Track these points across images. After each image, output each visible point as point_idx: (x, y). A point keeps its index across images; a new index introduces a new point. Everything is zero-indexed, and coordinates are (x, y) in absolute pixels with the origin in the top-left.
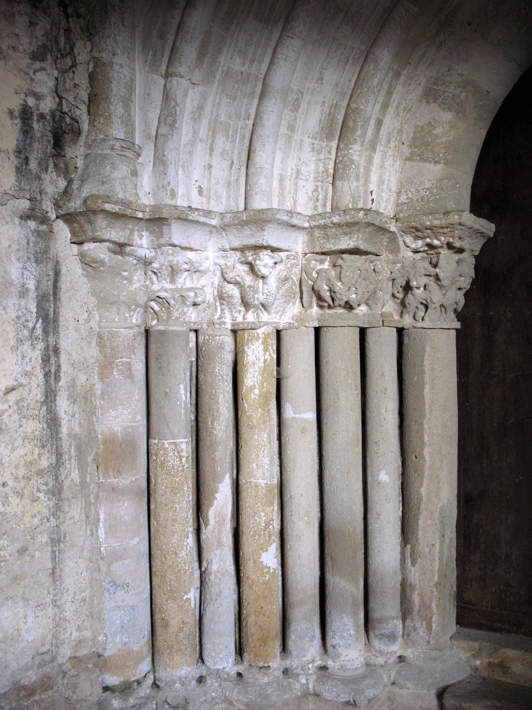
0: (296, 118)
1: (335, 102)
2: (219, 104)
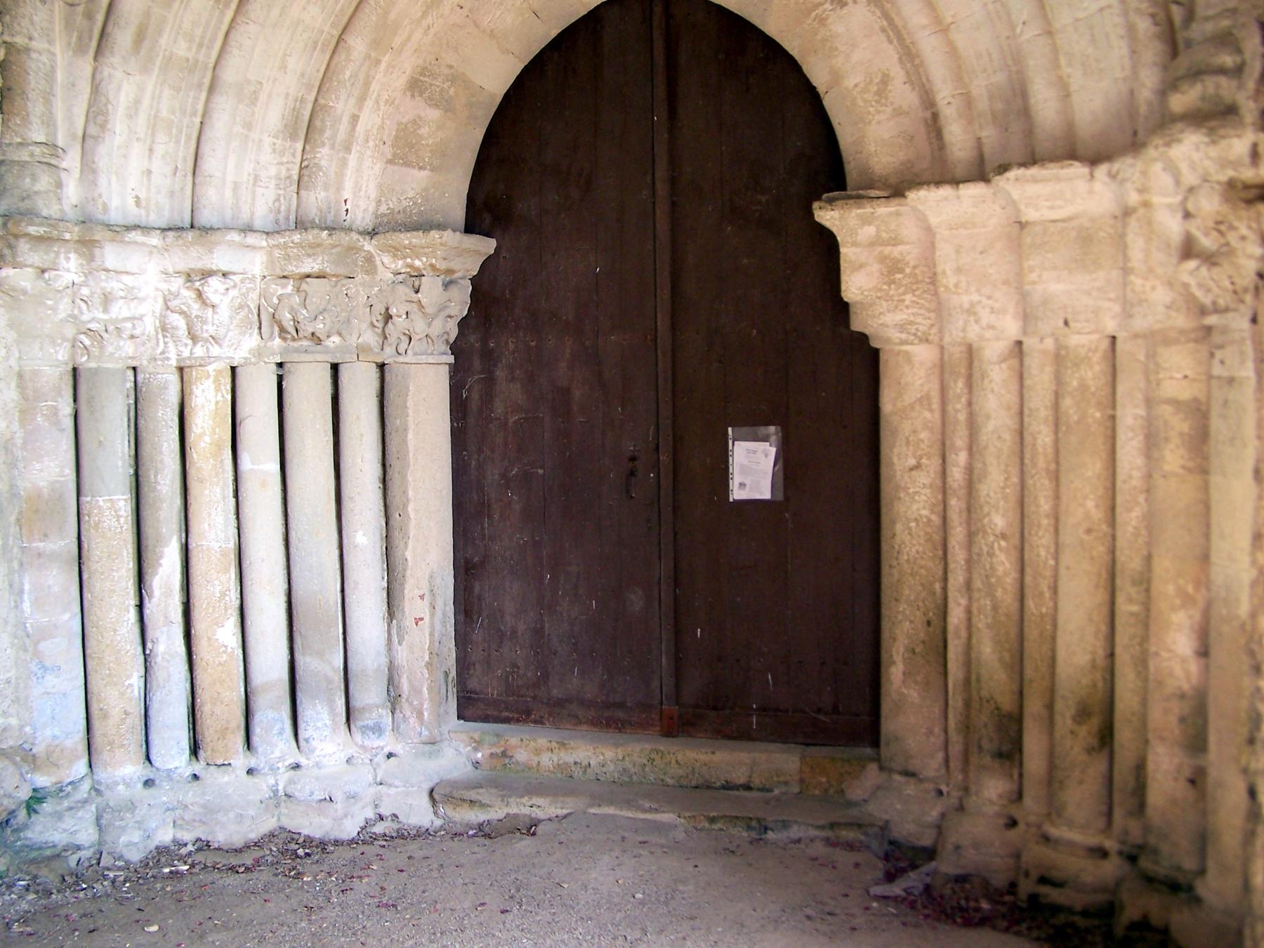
2: (160, 97)
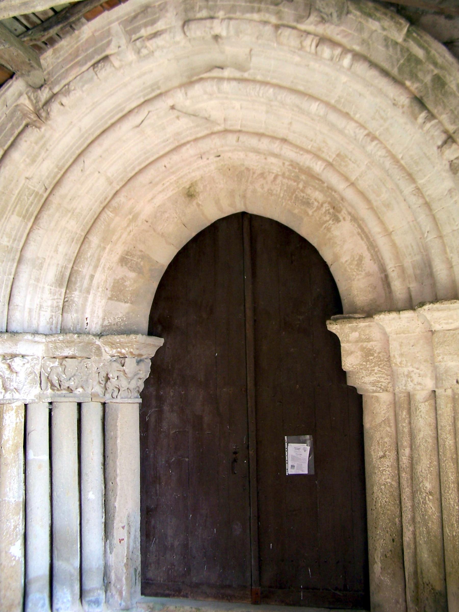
0: (40, 274)
1: (65, 264)
